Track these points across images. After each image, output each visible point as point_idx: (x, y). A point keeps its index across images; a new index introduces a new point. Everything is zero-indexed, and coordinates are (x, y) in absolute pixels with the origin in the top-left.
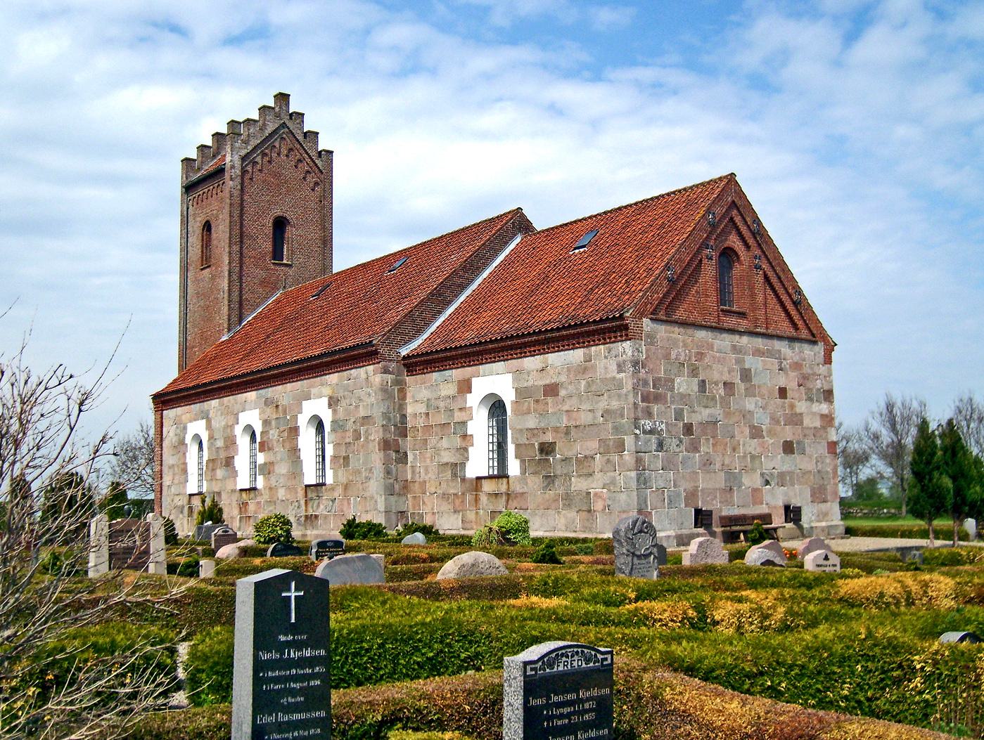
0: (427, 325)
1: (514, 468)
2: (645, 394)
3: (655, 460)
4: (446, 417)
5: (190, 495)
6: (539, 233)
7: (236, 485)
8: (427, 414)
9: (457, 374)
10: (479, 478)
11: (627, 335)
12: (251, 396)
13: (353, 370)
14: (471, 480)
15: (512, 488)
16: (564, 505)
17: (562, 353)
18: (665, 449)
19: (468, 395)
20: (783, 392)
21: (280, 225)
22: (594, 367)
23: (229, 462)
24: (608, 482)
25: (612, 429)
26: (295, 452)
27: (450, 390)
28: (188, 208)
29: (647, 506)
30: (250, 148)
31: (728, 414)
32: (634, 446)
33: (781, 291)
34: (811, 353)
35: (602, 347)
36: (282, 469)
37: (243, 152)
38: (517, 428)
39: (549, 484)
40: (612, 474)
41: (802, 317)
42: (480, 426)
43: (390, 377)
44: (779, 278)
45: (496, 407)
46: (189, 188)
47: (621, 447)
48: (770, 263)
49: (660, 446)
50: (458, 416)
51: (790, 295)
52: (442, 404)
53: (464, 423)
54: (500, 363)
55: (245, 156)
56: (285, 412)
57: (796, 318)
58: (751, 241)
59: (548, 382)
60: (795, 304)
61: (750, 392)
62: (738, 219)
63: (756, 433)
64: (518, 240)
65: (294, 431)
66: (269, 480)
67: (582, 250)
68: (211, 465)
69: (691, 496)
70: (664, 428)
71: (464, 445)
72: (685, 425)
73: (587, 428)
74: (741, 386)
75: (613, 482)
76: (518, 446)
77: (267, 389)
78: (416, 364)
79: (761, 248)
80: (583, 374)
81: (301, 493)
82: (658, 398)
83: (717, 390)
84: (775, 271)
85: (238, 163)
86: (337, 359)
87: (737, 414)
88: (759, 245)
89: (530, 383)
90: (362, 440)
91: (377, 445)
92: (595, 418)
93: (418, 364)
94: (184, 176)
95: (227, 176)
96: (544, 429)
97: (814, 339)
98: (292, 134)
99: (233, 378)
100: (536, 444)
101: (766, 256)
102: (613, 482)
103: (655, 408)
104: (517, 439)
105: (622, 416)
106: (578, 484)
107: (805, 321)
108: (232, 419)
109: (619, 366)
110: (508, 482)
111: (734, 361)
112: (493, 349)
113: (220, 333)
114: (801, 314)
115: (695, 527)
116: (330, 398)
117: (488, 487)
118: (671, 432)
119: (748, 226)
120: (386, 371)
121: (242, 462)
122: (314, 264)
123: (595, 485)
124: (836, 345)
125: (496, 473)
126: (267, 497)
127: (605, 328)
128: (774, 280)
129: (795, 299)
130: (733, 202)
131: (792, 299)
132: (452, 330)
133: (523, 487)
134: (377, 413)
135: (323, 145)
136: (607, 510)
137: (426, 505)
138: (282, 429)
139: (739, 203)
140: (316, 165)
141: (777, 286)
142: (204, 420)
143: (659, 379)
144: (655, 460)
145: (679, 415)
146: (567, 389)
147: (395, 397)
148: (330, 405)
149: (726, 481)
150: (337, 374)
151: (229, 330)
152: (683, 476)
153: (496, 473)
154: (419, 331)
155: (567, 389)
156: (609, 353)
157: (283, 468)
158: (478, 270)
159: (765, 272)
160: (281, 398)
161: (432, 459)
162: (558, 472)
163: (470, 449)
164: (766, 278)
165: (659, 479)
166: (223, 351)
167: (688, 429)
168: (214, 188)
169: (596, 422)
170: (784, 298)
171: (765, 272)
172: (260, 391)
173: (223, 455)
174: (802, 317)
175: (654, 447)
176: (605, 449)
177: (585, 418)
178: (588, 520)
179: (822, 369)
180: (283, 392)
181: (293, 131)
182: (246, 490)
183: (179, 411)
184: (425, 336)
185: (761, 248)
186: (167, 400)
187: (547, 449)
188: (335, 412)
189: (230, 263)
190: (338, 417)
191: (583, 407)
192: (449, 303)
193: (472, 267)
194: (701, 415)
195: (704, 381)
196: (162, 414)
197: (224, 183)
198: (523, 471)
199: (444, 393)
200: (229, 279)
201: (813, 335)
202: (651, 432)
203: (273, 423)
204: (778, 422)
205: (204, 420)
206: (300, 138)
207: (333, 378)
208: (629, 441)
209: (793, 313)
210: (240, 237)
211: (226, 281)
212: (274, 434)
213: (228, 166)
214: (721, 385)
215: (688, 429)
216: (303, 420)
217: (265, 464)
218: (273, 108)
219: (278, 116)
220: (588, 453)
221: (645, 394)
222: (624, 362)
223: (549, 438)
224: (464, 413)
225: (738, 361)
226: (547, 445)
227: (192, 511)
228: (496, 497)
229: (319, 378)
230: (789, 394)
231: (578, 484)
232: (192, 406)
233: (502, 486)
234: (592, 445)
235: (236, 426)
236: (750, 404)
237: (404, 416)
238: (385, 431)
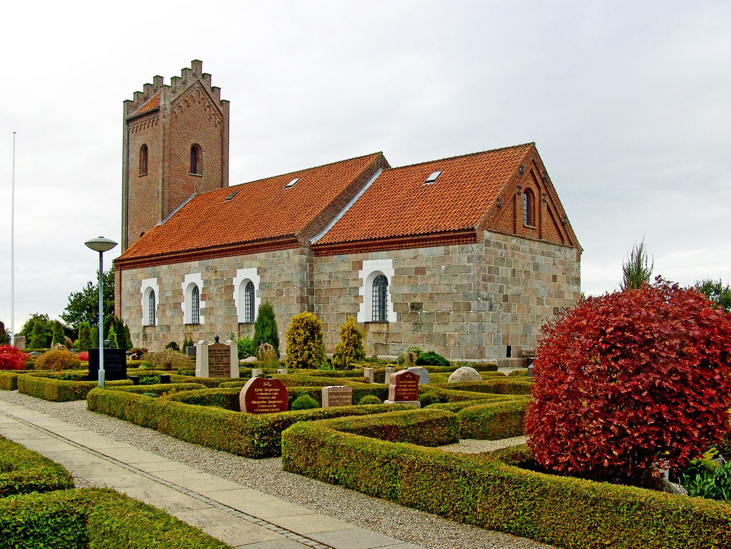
0: (327, 224)
1: (392, 316)
2: (484, 275)
3: (488, 316)
4: (343, 284)
5: (145, 327)
6: (392, 169)
7: (182, 321)
8: (329, 282)
9: (352, 257)
10: (366, 323)
11: (475, 240)
12: (195, 264)
13: (278, 251)
14: (361, 323)
15: (390, 329)
16: (427, 341)
17: (429, 248)
18: (493, 309)
19: (360, 271)
20: (555, 278)
21: (195, 149)
22: (451, 258)
23: (177, 306)
24: (459, 328)
25: (463, 297)
26: (231, 301)
27: (347, 267)
28: (128, 134)
29: (483, 343)
30: (176, 96)
31: (526, 290)
32: (477, 307)
33: (555, 216)
34: (571, 254)
35: (457, 246)
36: (220, 312)
37: (172, 99)
38: (396, 293)
39: (417, 328)
40: (462, 323)
41: (566, 233)
42: (367, 291)
43: (305, 257)
44: (555, 208)
45: (380, 281)
46: (128, 121)
47: (468, 307)
48: (551, 199)
49: (491, 307)
50: (353, 284)
51: (560, 219)
52: (340, 276)
53: (357, 288)
54: (383, 252)
55: (173, 102)
56: (222, 276)
57: (563, 233)
58: (541, 185)
59: (418, 266)
60: (563, 224)
61: (538, 277)
62: (535, 171)
63: (540, 302)
64: (380, 173)
65: (232, 288)
66: (209, 319)
67: (432, 183)
68: (161, 308)
69: (506, 338)
70: (493, 297)
71: (356, 302)
72: (504, 296)
73: (445, 295)
74: (533, 273)
75: (462, 328)
76: (395, 304)
77: (207, 260)
78: (321, 250)
79: (547, 190)
80: (443, 262)
81: (235, 328)
82: (490, 279)
83: (521, 276)
84: (553, 204)
85: (168, 107)
86: (266, 244)
87: (531, 290)
88: (546, 187)
89: (405, 266)
90: (284, 296)
91: (296, 300)
92: (451, 289)
93: (318, 250)
94: (126, 112)
95: (161, 115)
96: (414, 294)
97: (571, 246)
98: (204, 88)
99: (180, 252)
100: (409, 303)
101: (549, 194)
102: (462, 328)
103: (489, 284)
104: (395, 299)
105: (470, 289)
106: (437, 329)
107: (567, 235)
108: (179, 278)
109: (468, 258)
110: (388, 326)
111: (530, 258)
112: (379, 243)
113: (156, 220)
114: (565, 230)
115: (507, 357)
116: (259, 269)
117: (373, 328)
118: (496, 300)
119: (540, 176)
120: (302, 253)
121: (187, 306)
122: (217, 177)
123: (450, 330)
124: (583, 250)
125: (378, 320)
126: (208, 329)
127: (460, 235)
128: (552, 209)
129: (563, 221)
130: (533, 160)
131: (561, 221)
132: (346, 229)
133: (398, 330)
134: (296, 280)
135: (223, 97)
136: (457, 345)
137: (327, 338)
138: (219, 286)
139: (536, 161)
140: (218, 110)
141: (554, 213)
142: (156, 279)
143: (491, 267)
144: (488, 316)
145: (501, 290)
146: (432, 270)
147: (310, 269)
148: (258, 273)
149: (523, 330)
150: (264, 253)
151: (163, 219)
152: (502, 327)
153: (378, 320)
154: (322, 229)
155: (432, 270)
156: (462, 250)
157: (221, 311)
158: (356, 192)
159: (547, 204)
160: (219, 266)
161: (332, 310)
162: (424, 321)
163: (361, 305)
164: (548, 208)
165: (489, 327)
166: (159, 234)
167: (506, 298)
168: (150, 122)
169: (451, 292)
170: (557, 220)
171: (547, 204)
172: (202, 261)
173: (172, 301)
174: (566, 233)
175: (487, 308)
176: (457, 308)
177: (443, 289)
178: (444, 350)
179: (576, 264)
180: (222, 263)
181: (204, 87)
182: (190, 325)
183: (134, 271)
184: (325, 232)
185: (547, 190)
186: (125, 264)
187: (416, 307)
188: (262, 277)
189: (163, 174)
190: (265, 281)
191: (442, 282)
192: (339, 211)
193: (353, 189)
194: (511, 290)
195: (514, 270)
196: (121, 272)
197: (158, 119)
198: (399, 319)
199: (341, 269)
200: (163, 185)
201: (572, 244)
202: (486, 299)
203: (213, 282)
204: (551, 296)
205: (156, 279)
206: (209, 91)
207: (262, 256)
208: (474, 304)
209: (561, 229)
210: (169, 156)
211: (160, 186)
212: (213, 290)
213: (161, 109)
214: (523, 272)
215: (506, 298)
216: (237, 282)
217: (206, 309)
218: (191, 70)
219: (194, 75)
220: (445, 310)
221: (484, 275)
222: (472, 256)
223: (418, 300)
224: (357, 282)
225: (533, 258)
226: (416, 304)
227: (146, 337)
228: (379, 335)
229: (250, 255)
230: (558, 279)
231: (437, 329)
232: (146, 268)
233: (384, 328)
234: (448, 306)
235: (183, 283)
236: (537, 284)
237: (312, 283)
238: (301, 291)
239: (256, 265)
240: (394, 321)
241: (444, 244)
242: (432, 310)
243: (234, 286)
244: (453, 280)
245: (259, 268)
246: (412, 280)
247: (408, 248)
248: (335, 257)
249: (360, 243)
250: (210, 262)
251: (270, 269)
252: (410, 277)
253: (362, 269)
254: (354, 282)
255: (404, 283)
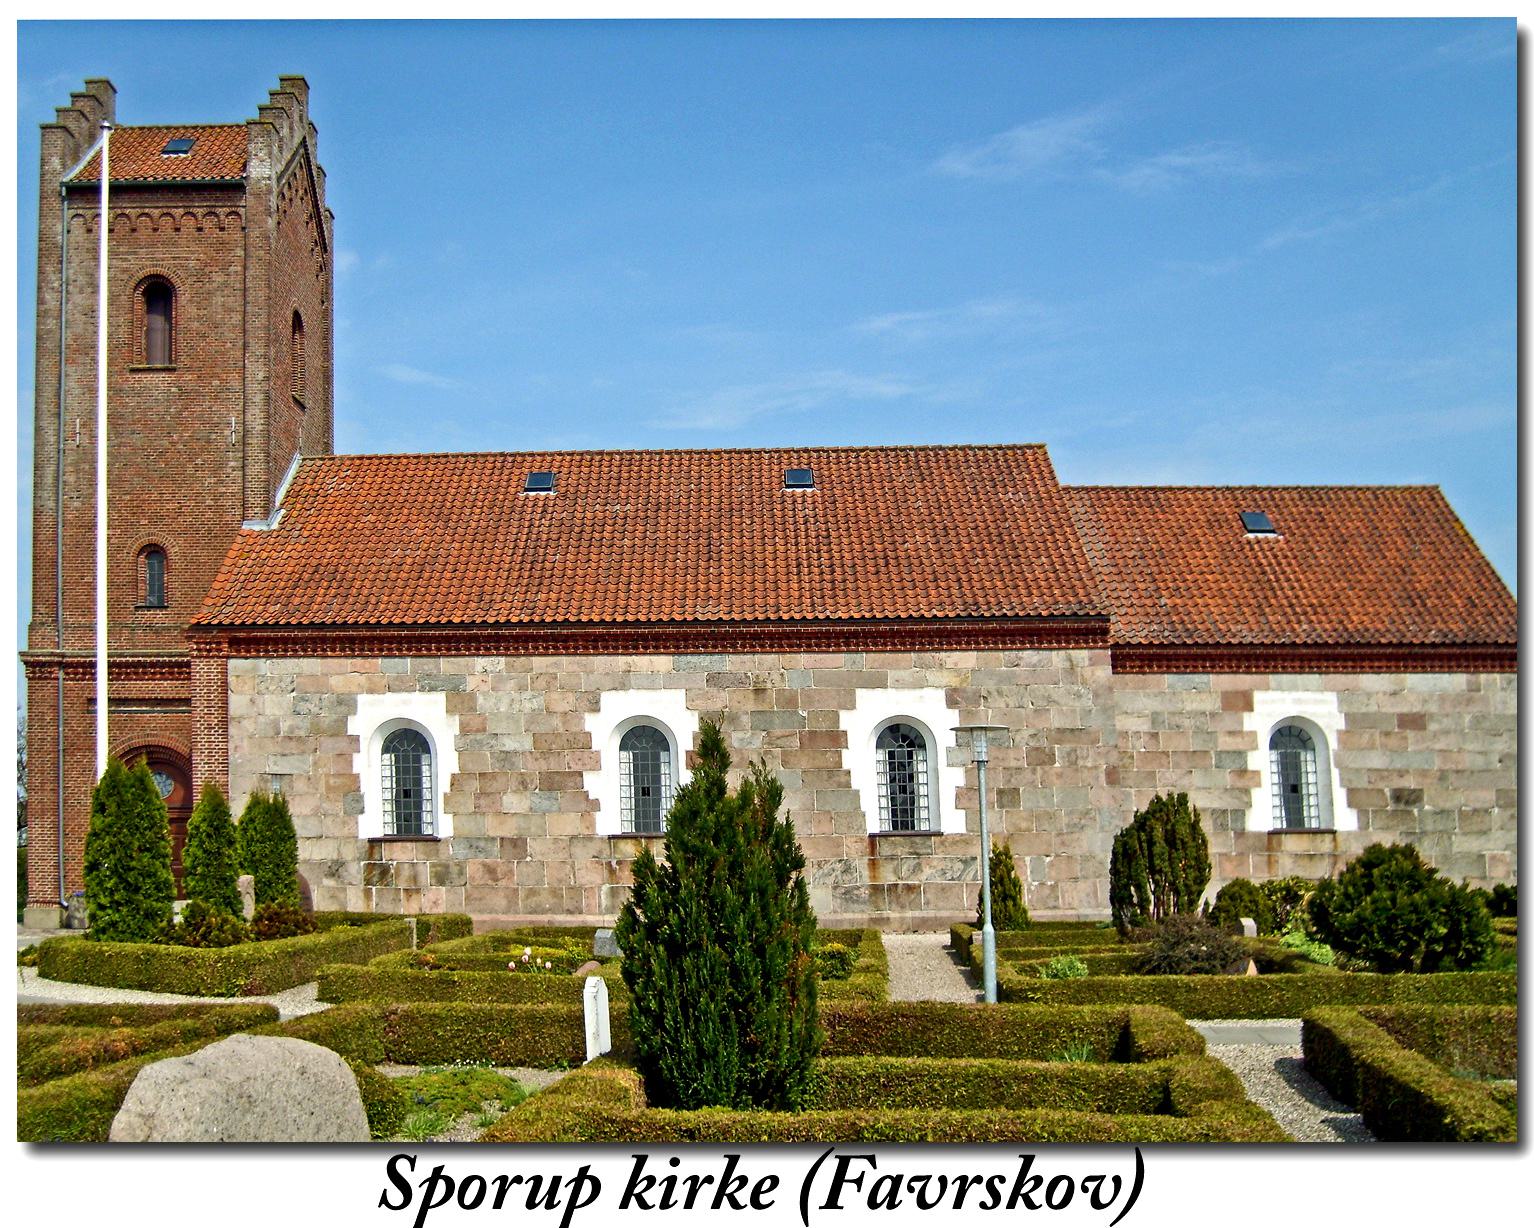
14: (1258, 835)
27: (1212, 704)
45: (1292, 738)
50: (1225, 743)
52: (1187, 723)
53: (1240, 754)
71: (1240, 784)
80: (1467, 705)
89: (1373, 708)
90: (1057, 765)
146: (1440, 722)
162: (1429, 827)
177: (1468, 761)
207: (965, 660)
223: (1410, 783)
224: (1239, 740)
239: (945, 681)
240: (868, 827)
241: (1467, 670)
242: (1448, 805)
243: (845, 733)
244: (1491, 744)
245: (955, 690)
246: (1393, 742)
247: (1378, 671)
248: (1168, 679)
249: (1356, 652)
250: (730, 663)
251: (1000, 693)
252: (1387, 734)
253: (853, 707)
254: (1229, 739)
255: (1372, 747)
